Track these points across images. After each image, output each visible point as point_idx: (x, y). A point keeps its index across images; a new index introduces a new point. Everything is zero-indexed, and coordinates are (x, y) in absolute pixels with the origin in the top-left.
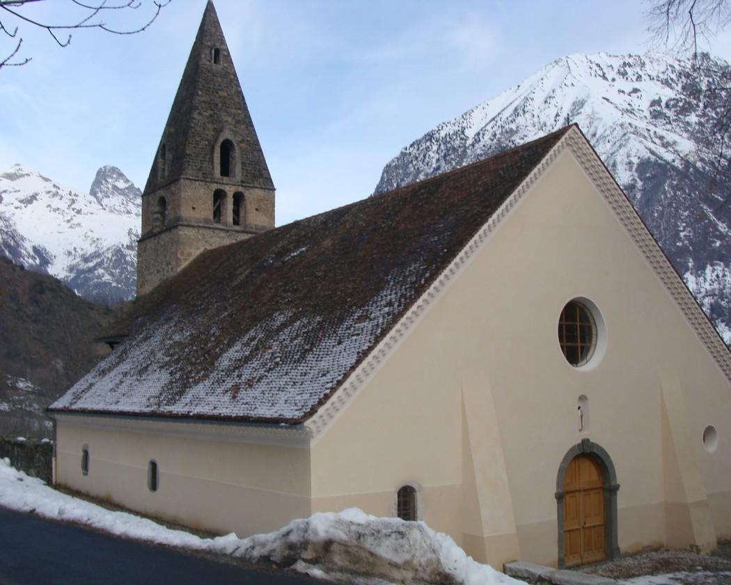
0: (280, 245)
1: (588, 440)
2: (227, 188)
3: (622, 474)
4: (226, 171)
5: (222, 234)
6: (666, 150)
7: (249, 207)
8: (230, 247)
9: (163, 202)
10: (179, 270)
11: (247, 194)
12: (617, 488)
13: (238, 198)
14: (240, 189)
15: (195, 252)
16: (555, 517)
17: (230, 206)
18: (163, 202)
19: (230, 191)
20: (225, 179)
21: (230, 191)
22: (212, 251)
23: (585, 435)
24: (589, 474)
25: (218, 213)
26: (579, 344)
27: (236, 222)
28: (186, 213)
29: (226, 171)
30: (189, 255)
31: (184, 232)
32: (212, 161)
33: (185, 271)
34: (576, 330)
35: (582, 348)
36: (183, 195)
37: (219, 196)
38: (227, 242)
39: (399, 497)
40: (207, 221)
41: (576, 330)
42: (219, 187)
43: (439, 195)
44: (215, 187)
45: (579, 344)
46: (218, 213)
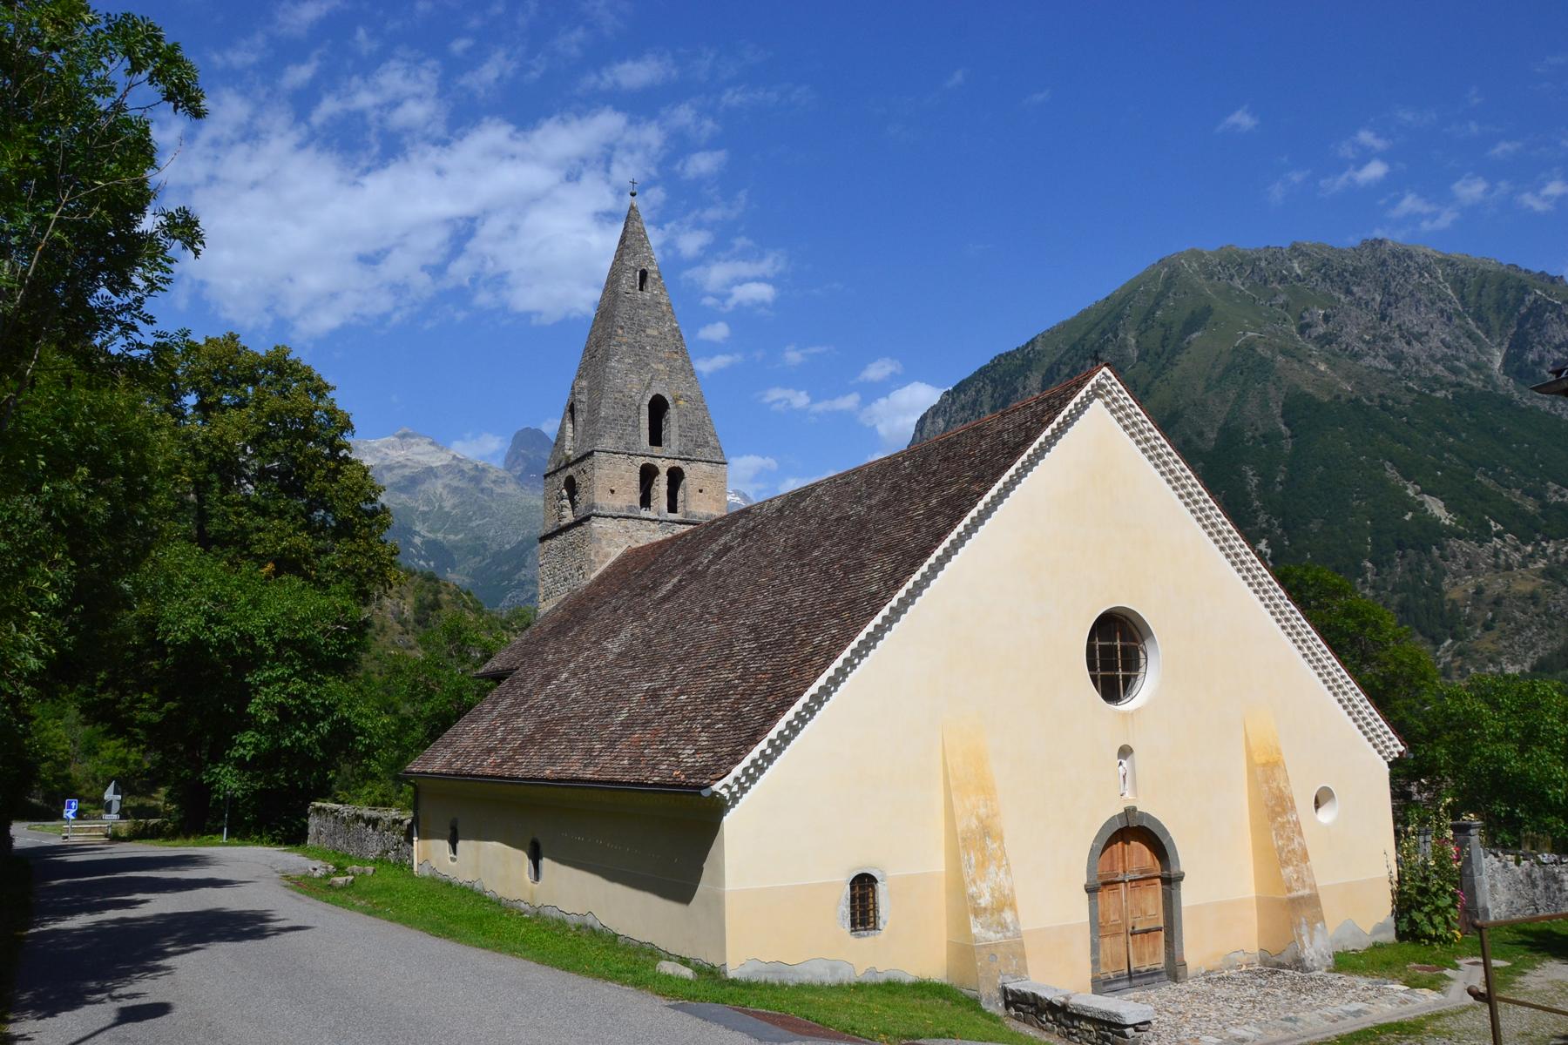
0: (722, 541)
1: (1134, 809)
2: (658, 463)
3: (1186, 857)
4: (656, 438)
5: (652, 526)
6: (190, 337)
7: (689, 489)
8: (660, 544)
9: (571, 485)
10: (593, 576)
11: (686, 468)
12: (1181, 877)
13: (675, 477)
14: (678, 463)
15: (615, 553)
16: (1087, 919)
17: (661, 486)
18: (571, 485)
19: (663, 466)
20: (656, 450)
21: (663, 466)
22: (637, 550)
23: (1130, 799)
24: (1139, 855)
25: (645, 501)
26: (1120, 673)
27: (672, 508)
28: (603, 501)
29: (656, 438)
30: (607, 556)
31: (597, 524)
32: (637, 426)
33: (601, 579)
34: (1116, 650)
35: (1127, 680)
36: (597, 472)
37: (648, 474)
38: (659, 537)
39: (852, 888)
40: (630, 508)
41: (1116, 650)
42: (648, 460)
43: (1321, 468)
44: (641, 461)
45: (1120, 673)
46: (645, 501)
